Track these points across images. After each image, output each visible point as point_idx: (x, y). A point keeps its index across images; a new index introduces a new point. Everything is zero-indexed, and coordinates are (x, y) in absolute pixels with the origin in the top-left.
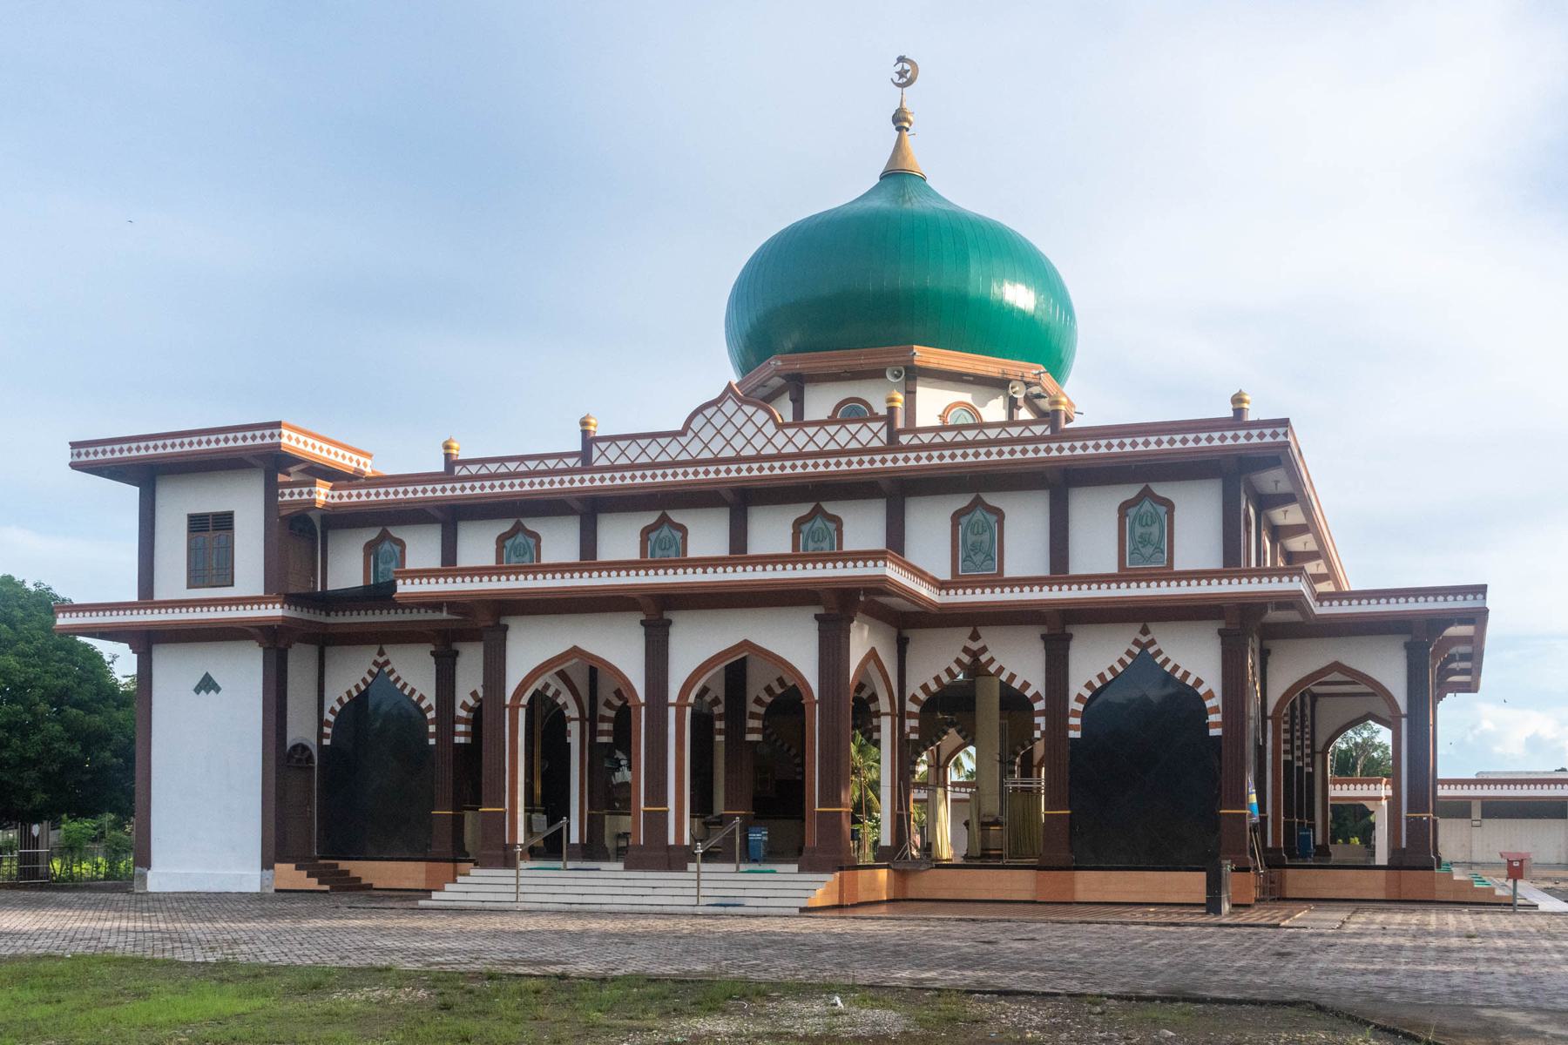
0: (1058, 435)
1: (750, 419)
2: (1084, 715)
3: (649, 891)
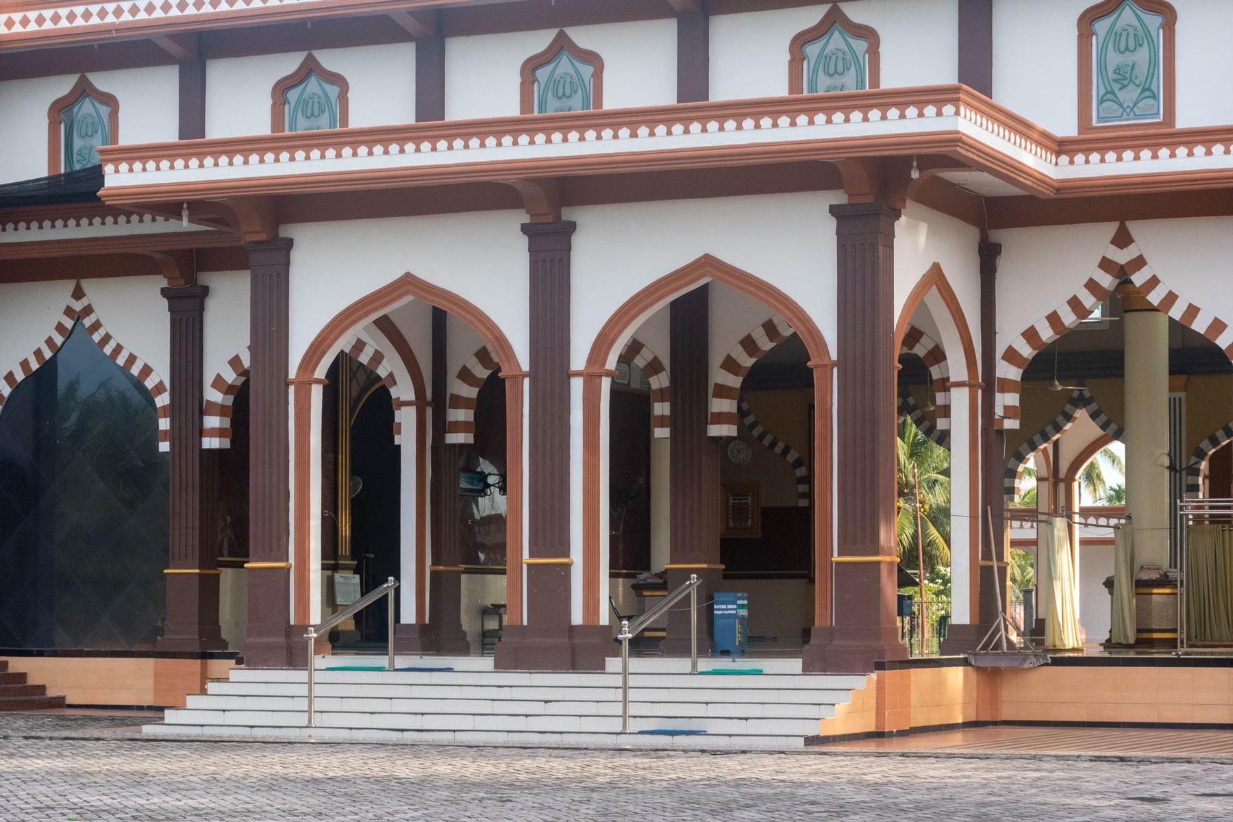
3: (539, 708)
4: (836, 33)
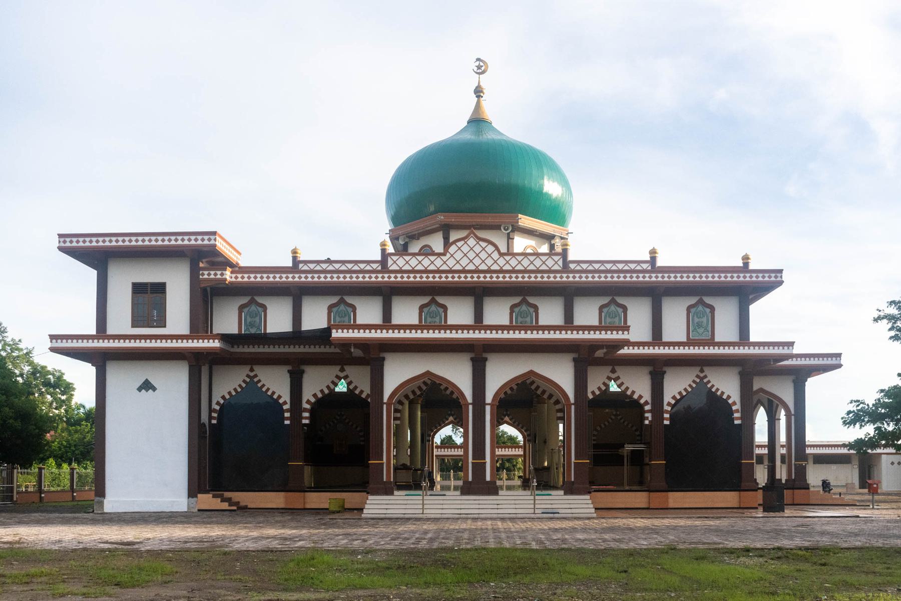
0: (566, 268)
1: (484, 249)
2: (311, 411)
3: (496, 506)
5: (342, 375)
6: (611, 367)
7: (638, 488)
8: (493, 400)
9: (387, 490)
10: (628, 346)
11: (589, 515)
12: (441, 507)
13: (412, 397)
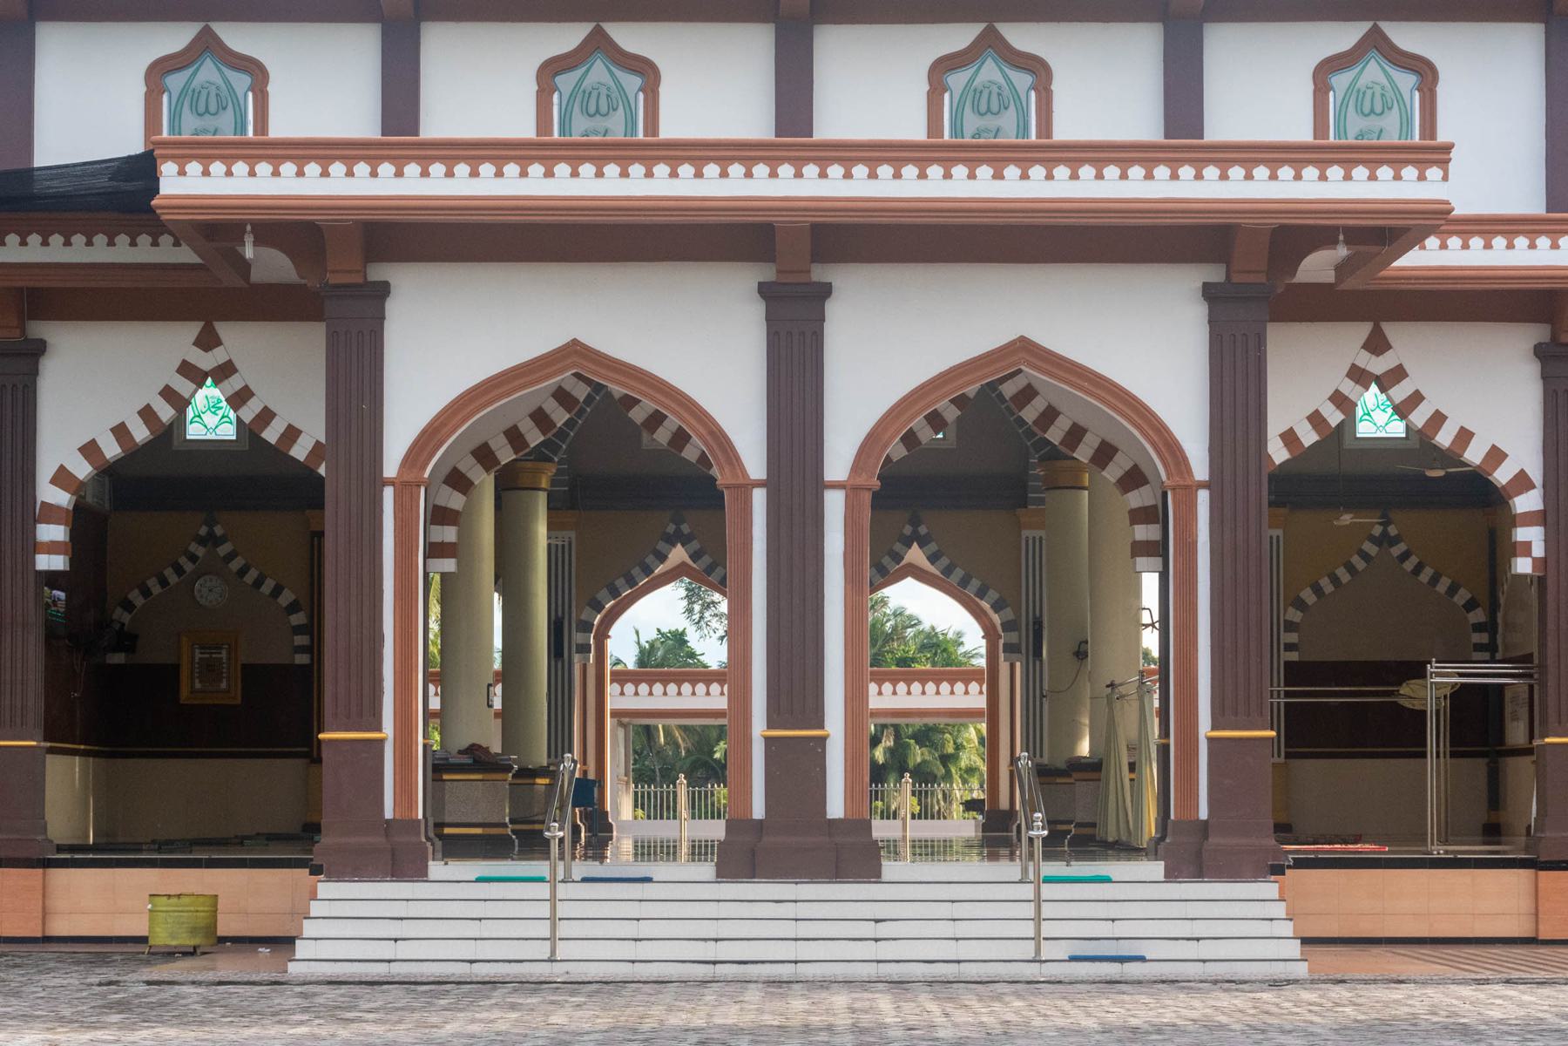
2: (83, 520)
3: (868, 930)
4: (989, 62)
5: (206, 361)
6: (1365, 329)
7: (1479, 850)
8: (856, 468)
9: (398, 858)
10: (1444, 235)
11: (1279, 971)
12: (629, 929)
13: (506, 455)
